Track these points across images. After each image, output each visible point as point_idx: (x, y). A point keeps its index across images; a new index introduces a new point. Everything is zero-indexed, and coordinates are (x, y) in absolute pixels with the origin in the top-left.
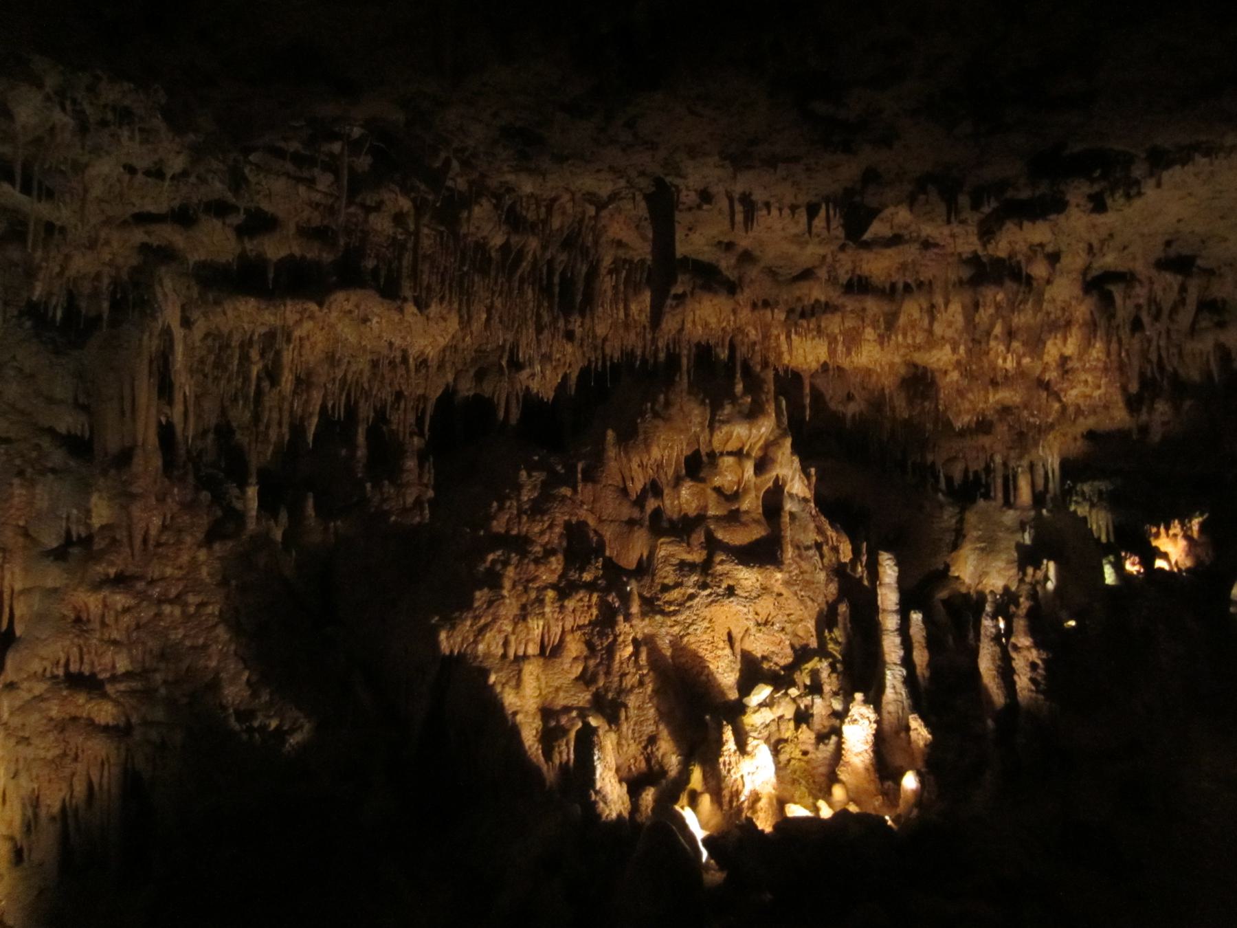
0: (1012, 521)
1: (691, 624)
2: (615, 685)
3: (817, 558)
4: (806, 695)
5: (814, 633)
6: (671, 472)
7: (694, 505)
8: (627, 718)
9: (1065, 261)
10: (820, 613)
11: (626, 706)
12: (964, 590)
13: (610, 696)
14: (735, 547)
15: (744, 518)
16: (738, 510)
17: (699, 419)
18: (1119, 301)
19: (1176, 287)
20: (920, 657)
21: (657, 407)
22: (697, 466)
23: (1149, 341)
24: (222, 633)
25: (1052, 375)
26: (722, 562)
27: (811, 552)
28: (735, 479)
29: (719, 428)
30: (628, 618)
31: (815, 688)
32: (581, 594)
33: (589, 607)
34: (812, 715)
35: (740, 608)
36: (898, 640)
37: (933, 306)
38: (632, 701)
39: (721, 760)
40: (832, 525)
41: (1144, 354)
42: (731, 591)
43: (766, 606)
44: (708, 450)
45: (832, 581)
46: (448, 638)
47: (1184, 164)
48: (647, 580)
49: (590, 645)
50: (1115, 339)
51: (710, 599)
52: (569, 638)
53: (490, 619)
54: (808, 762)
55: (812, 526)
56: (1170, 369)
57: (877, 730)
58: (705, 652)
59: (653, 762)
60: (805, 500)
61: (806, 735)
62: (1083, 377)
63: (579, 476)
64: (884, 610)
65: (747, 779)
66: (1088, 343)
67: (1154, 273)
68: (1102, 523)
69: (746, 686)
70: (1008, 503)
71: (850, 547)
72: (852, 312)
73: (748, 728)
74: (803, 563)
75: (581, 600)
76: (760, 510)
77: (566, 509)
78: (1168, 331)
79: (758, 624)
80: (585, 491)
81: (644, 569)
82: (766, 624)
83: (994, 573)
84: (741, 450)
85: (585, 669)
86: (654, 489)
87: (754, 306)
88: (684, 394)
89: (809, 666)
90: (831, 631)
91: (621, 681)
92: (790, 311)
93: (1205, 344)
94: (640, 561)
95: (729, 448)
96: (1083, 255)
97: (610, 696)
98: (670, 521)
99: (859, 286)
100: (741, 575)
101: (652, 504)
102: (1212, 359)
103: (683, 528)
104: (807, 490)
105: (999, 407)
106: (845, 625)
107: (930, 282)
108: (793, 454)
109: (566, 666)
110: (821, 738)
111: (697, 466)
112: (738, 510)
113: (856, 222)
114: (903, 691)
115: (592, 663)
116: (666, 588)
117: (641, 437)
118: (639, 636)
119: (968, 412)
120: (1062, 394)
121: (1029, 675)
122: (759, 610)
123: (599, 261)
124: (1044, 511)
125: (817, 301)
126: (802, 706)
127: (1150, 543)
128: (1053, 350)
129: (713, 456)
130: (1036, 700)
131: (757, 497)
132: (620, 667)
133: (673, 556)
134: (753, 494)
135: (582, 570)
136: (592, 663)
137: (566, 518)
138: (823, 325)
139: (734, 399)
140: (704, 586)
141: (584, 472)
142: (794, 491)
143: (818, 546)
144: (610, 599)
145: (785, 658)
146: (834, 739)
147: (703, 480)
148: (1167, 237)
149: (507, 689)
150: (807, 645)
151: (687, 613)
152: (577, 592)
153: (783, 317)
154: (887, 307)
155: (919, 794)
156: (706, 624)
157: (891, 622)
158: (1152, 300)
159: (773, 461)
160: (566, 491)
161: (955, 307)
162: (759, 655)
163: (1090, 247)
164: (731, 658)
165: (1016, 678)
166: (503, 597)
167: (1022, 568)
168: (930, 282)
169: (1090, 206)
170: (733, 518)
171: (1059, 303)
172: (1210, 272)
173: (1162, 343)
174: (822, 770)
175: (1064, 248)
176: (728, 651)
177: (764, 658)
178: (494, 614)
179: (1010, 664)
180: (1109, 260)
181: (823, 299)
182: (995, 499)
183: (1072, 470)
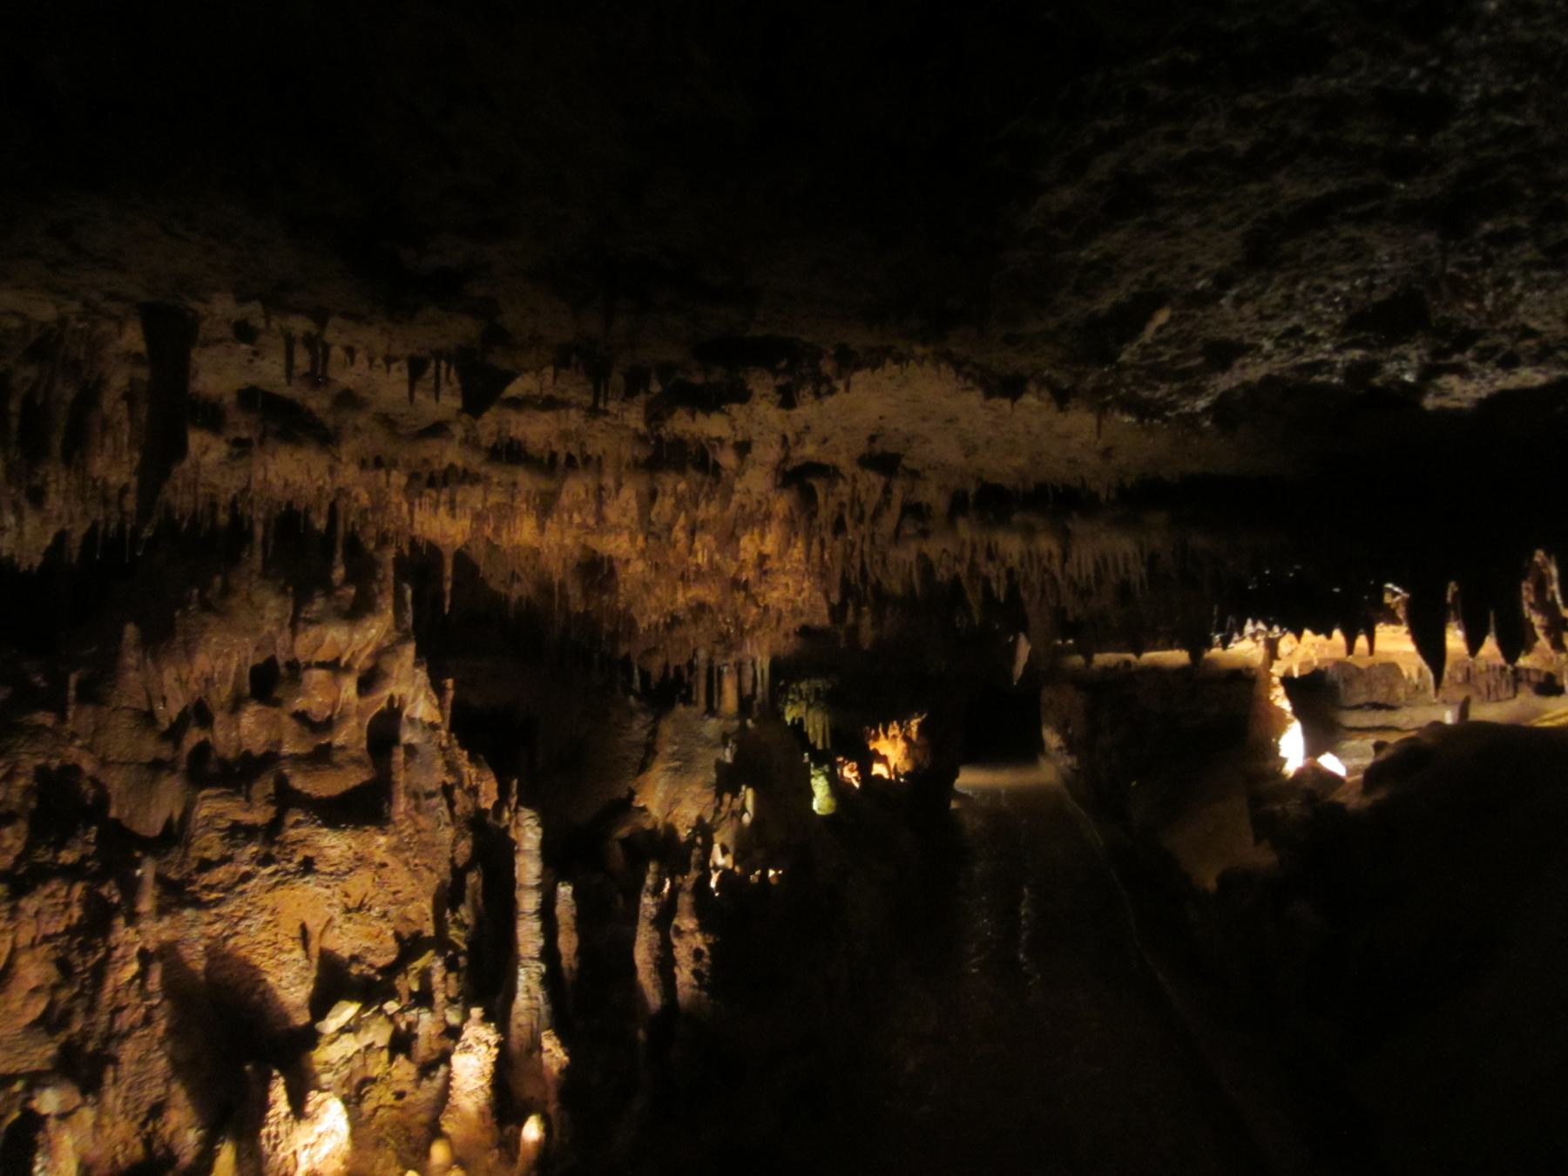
0: (711, 732)
1: (242, 918)
2: (101, 1028)
3: (444, 808)
4: (411, 1008)
5: (430, 916)
6: (226, 690)
7: (261, 739)
8: (115, 1080)
9: (757, 452)
10: (442, 886)
11: (115, 1061)
12: (648, 826)
13: (90, 1046)
14: (320, 799)
16: (329, 745)
17: (276, 615)
18: (821, 499)
19: (879, 489)
20: (567, 943)
21: (208, 595)
22: (268, 682)
23: (853, 545)
25: (749, 574)
26: (297, 824)
27: (435, 801)
28: (328, 700)
29: (305, 630)
30: (132, 918)
31: (424, 999)
32: (54, 885)
33: (67, 905)
34: (416, 1036)
35: (322, 890)
36: (537, 926)
37: (601, 488)
38: (128, 1051)
39: (264, 1131)
40: (472, 759)
41: (847, 558)
42: (308, 866)
43: (361, 884)
44: (289, 658)
45: (464, 837)
47: (874, 368)
48: (176, 855)
49: (64, 966)
50: (816, 542)
51: (274, 880)
52: (23, 960)
54: (403, 1109)
55: (439, 762)
56: (873, 579)
57: (499, 1056)
58: (262, 960)
59: (155, 1145)
60: (433, 727)
61: (404, 1070)
62: (784, 579)
63: (72, 693)
64: (522, 887)
65: (303, 1158)
66: (788, 543)
67: (857, 470)
68: (819, 727)
69: (321, 1004)
70: (711, 711)
71: (495, 786)
72: (499, 484)
73: (318, 1068)
74: (420, 819)
75: (52, 895)
76: (364, 745)
77: (41, 747)
78: (872, 536)
79: (348, 910)
80: (80, 718)
81: (174, 836)
82: (359, 909)
83: (687, 802)
84: (338, 660)
85: (51, 1006)
86: (200, 713)
87: (363, 465)
88: (254, 577)
89: (419, 964)
90: (455, 910)
91: (112, 1021)
92: (414, 477)
93: (906, 554)
94: (168, 824)
95: (320, 657)
96: (777, 448)
97: (90, 1046)
98: (223, 762)
99: (510, 453)
100: (325, 842)
101: (194, 737)
102: (915, 574)
103: (238, 773)
104: (437, 712)
105: (694, 604)
106: (475, 902)
107: (599, 458)
108: (417, 664)
109: (16, 1005)
110: (426, 1069)
111: (268, 682)
112: (329, 745)
113: (482, 391)
114: (540, 995)
115: (64, 994)
116: (206, 865)
117: (180, 638)
118: (151, 946)
119: (655, 610)
120: (760, 599)
121: (692, 966)
122: (350, 890)
123: (102, 382)
124: (749, 722)
125: (452, 466)
126: (403, 1026)
127: (867, 746)
128: (749, 545)
129: (295, 669)
130: (698, 997)
131: (359, 725)
132: (114, 998)
133: (221, 816)
134: (353, 722)
135: (60, 845)
136: (64, 994)
137: (40, 761)
138: (459, 498)
139: (329, 590)
140: (266, 860)
141: (81, 686)
142: (418, 715)
143: (447, 790)
144: (104, 891)
145: (386, 954)
146: (443, 1069)
147: (277, 703)
148: (870, 432)
150: (420, 933)
151: (237, 902)
152: (45, 884)
153: (403, 481)
154: (544, 484)
155: (545, 1146)
156: (266, 917)
157: (529, 902)
158: (855, 499)
159: (386, 675)
160: (45, 718)
161: (628, 494)
162: (346, 955)
163: (785, 438)
164: (303, 963)
165: (676, 970)
167: (719, 795)
168: (599, 458)
169: (779, 397)
170: (321, 757)
171: (755, 496)
172: (915, 474)
173: (866, 548)
174: (423, 1117)
175: (755, 438)
176: (298, 953)
177: (355, 959)
179: (672, 955)
180: (809, 450)
181: (459, 463)
182: (696, 704)
183: (784, 672)
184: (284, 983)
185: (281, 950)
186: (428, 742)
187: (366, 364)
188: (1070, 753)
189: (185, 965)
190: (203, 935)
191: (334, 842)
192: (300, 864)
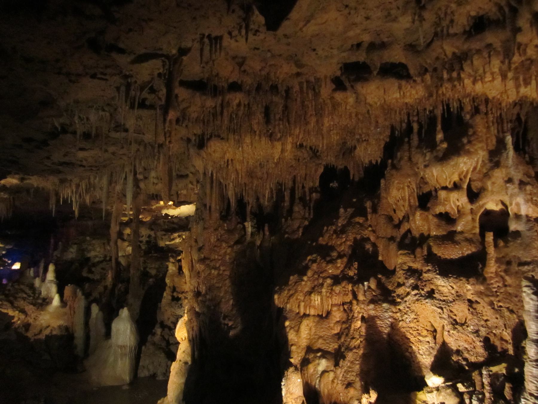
15: (458, 238)
24: (228, 282)
38: (350, 356)
42: (431, 295)
46: (278, 298)
53: (294, 292)
74: (507, 278)
91: (350, 342)
111: (425, 200)
116: (399, 285)
131: (473, 219)
149: (292, 331)
160: (361, 220)
164: (432, 345)
166: (303, 280)
170: (450, 238)
176: (429, 339)
177: (458, 352)
178: (296, 289)
184: (421, 352)
185: (419, 334)
186: (529, 230)
187: (228, 36)
188: (280, 311)
189: (377, 328)
190: (391, 317)
191: (443, 284)
192: (428, 292)
